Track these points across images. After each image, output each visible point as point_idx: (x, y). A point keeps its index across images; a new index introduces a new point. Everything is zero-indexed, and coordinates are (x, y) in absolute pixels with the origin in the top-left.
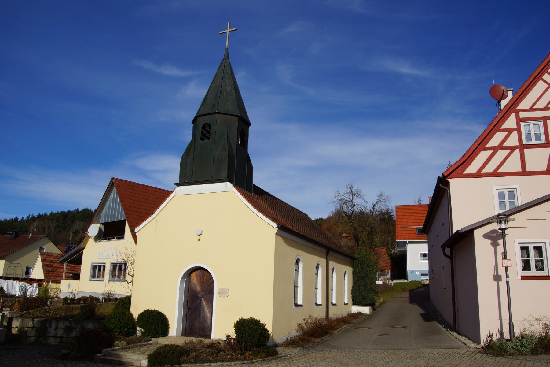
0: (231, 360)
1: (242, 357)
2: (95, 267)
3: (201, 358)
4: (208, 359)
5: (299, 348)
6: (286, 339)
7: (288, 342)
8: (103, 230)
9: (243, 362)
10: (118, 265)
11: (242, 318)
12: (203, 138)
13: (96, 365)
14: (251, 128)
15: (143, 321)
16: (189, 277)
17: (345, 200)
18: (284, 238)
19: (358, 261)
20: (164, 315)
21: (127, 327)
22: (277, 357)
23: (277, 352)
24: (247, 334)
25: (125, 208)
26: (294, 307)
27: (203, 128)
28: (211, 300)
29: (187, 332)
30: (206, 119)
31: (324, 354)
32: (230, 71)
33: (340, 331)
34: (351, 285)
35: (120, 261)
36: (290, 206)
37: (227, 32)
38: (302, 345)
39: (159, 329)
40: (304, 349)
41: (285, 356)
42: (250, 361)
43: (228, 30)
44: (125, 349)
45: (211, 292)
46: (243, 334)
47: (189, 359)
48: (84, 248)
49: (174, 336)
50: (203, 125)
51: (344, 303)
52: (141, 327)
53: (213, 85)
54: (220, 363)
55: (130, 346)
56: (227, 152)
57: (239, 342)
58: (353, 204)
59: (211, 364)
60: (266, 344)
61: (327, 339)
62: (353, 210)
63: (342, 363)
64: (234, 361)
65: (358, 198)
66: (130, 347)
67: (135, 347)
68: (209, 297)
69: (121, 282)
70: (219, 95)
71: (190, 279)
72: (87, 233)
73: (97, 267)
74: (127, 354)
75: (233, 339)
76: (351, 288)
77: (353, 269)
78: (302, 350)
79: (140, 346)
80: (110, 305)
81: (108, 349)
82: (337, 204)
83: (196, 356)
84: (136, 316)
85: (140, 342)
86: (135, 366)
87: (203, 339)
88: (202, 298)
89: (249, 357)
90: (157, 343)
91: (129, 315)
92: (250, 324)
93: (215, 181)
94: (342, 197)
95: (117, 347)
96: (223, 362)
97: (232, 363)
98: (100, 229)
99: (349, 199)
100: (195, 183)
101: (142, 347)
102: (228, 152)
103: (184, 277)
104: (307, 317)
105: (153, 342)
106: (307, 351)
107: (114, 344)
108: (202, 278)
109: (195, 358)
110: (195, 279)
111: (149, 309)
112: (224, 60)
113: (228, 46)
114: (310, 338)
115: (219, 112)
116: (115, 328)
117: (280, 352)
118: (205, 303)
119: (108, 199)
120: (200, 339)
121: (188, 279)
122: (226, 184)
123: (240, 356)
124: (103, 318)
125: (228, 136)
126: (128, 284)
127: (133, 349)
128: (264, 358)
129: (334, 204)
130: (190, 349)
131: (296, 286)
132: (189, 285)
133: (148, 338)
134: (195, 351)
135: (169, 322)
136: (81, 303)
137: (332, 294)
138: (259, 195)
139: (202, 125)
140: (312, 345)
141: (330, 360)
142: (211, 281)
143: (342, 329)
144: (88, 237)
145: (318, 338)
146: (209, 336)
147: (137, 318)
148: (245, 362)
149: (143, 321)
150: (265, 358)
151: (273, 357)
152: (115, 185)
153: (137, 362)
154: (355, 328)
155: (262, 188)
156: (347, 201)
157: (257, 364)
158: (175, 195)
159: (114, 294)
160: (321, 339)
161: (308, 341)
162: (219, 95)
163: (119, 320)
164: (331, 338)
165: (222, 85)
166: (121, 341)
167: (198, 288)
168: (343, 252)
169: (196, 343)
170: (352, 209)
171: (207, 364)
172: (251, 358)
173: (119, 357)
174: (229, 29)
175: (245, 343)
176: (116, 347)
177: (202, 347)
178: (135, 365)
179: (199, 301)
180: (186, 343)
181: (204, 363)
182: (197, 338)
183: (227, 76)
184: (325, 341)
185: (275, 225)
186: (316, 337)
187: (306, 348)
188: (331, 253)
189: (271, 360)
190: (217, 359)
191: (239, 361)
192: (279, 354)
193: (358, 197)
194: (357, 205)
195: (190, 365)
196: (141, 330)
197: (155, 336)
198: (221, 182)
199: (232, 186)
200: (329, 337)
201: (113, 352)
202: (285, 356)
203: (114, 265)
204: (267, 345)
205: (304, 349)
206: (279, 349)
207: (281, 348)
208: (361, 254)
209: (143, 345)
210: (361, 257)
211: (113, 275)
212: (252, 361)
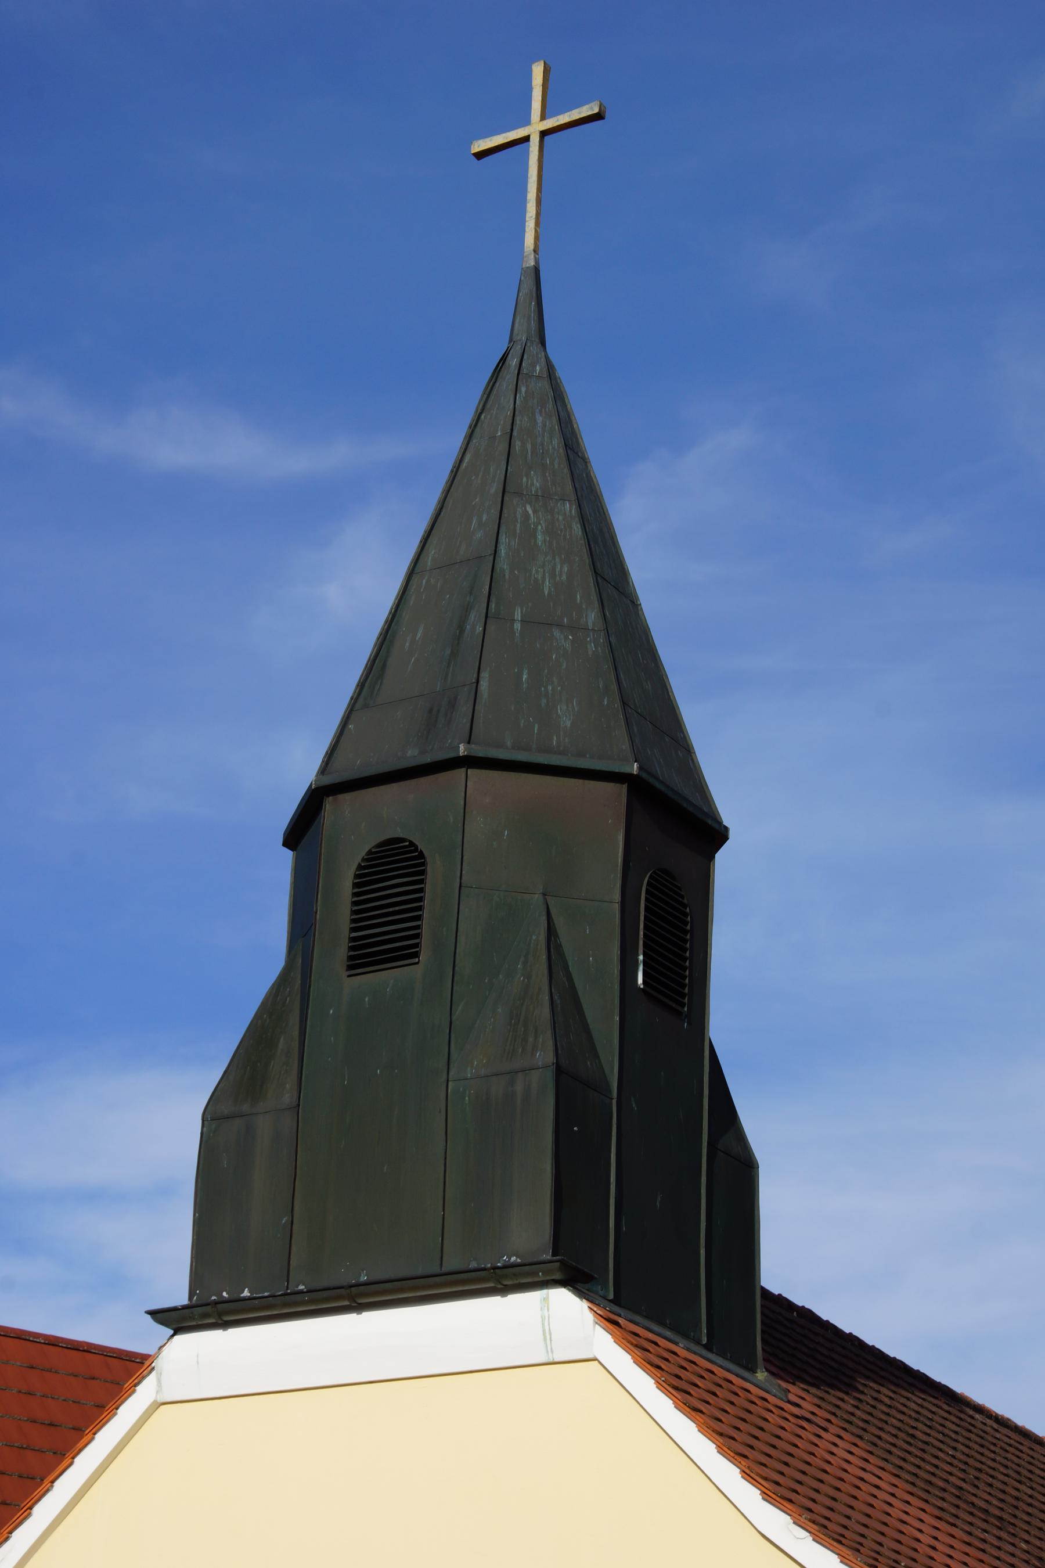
27: (364, 880)
32: (557, 442)
37: (526, 139)
43: (535, 127)
50: (363, 853)
53: (431, 552)
56: (544, 1056)
70: (475, 624)
100: (311, 1302)
102: (550, 1058)
112: (513, 362)
122: (546, 1299)
125: (551, 932)
138: (815, 1382)
139: (358, 860)
155: (846, 1324)
158: (157, 1405)
162: (475, 624)
165: (503, 550)
174: (543, 117)
183: (535, 482)
198: (504, 1290)
199: (590, 1317)
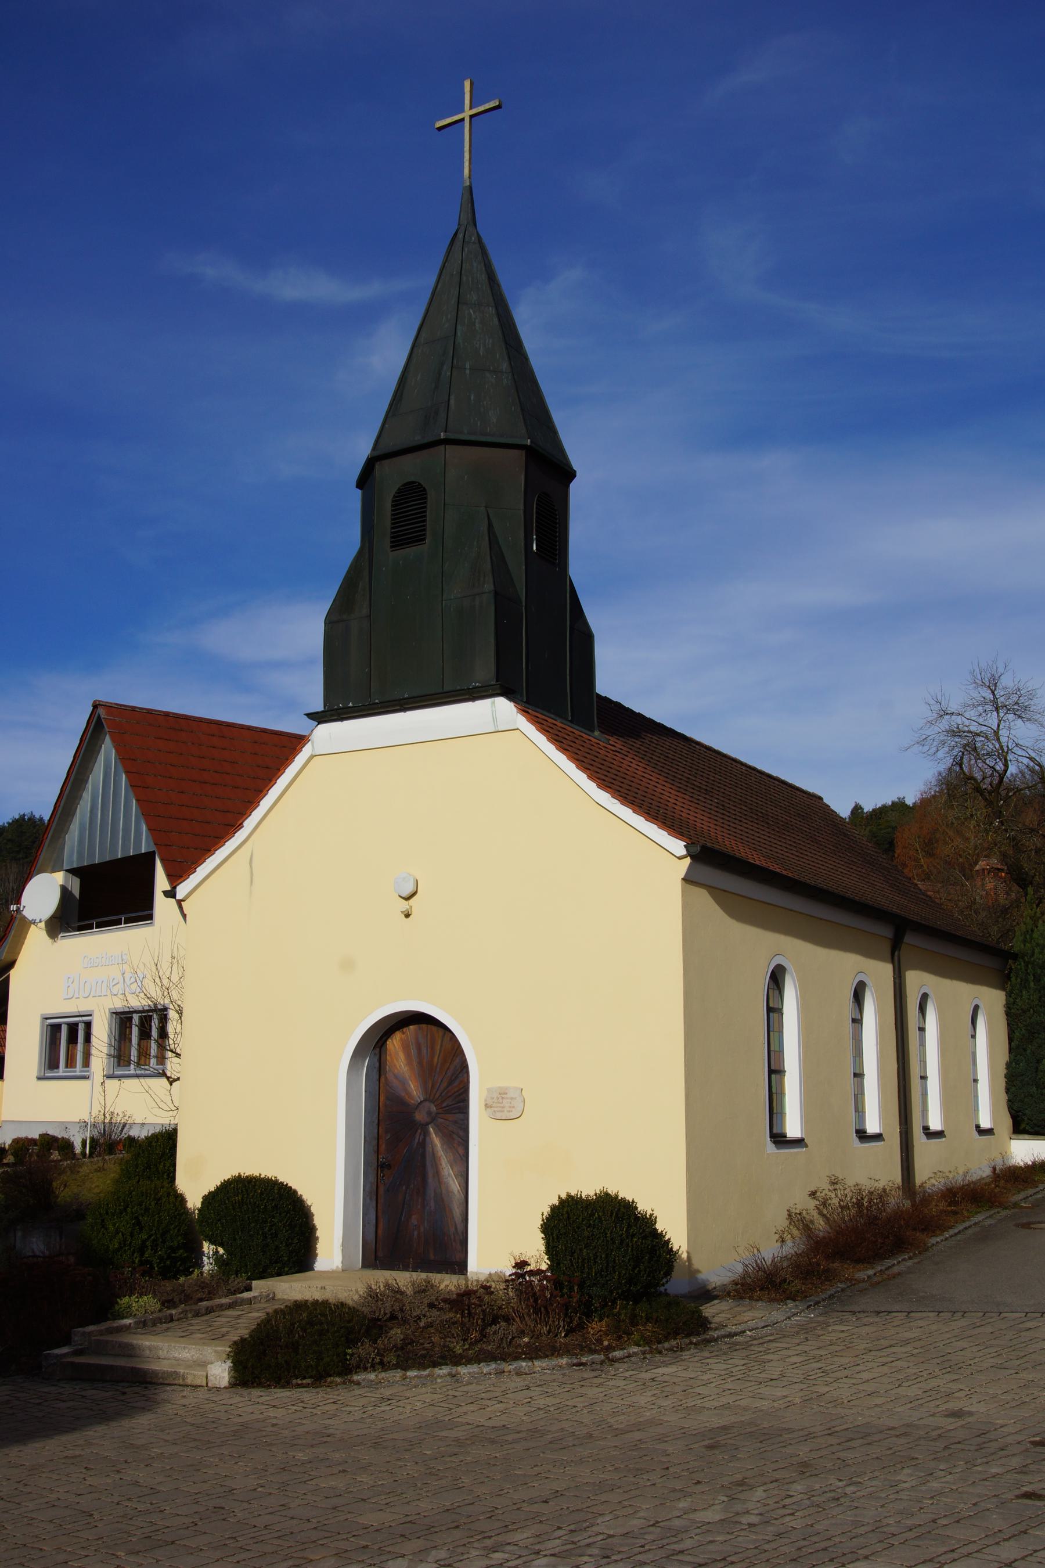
0: (533, 1353)
1: (576, 1338)
2: (55, 1029)
3: (424, 1349)
4: (450, 1350)
5: (791, 1304)
6: (740, 1269)
7: (749, 1280)
8: (76, 893)
9: (575, 1361)
10: (136, 1018)
11: (569, 1195)
12: (399, 541)
13: (46, 1390)
14: (576, 490)
15: (219, 1220)
16: (378, 1049)
17: (969, 732)
18: (718, 894)
19: (1027, 964)
20: (295, 1192)
21: (164, 1242)
22: (703, 1337)
23: (706, 1318)
24: (588, 1254)
25: (149, 810)
26: (771, 1148)
27: (397, 503)
28: (461, 1133)
29: (380, 1254)
30: (408, 468)
31: (883, 1327)
32: (483, 277)
33: (959, 1237)
34: (1004, 1057)
35: (137, 1002)
36: (750, 767)
37: (463, 120)
38: (803, 1292)
39: (277, 1248)
40: (808, 1307)
41: (736, 1334)
42: (602, 1357)
43: (467, 113)
44: (154, 1325)
45: (461, 1104)
46: (572, 1254)
47: (378, 1354)
48: (11, 964)
49: (334, 1268)
51: (978, 1127)
52: (212, 1242)
54: (493, 1366)
55: (173, 1312)
56: (489, 587)
57: (558, 1284)
58: (1001, 747)
59: (459, 1368)
60: (662, 1289)
61: (902, 1267)
62: (1003, 767)
63: (947, 1365)
64: (541, 1357)
65: (1020, 720)
66: (171, 1315)
67: (189, 1315)
68: (456, 1122)
69: (142, 1080)
71: (382, 1059)
72: (18, 910)
73: (64, 1030)
74: (160, 1344)
75: (539, 1272)
76: (1002, 1070)
77: (1009, 995)
78: (803, 1311)
79: (209, 1311)
80: (112, 1166)
81: (91, 1328)
82: (938, 750)
83: (407, 1342)
84: (194, 1201)
85: (211, 1295)
86: (187, 1386)
87: (436, 1278)
88: (427, 1124)
89: (600, 1341)
90: (271, 1298)
91: (172, 1199)
92: (599, 1218)
93: (453, 696)
94: (959, 720)
95: (126, 1317)
96: (504, 1360)
97: (537, 1363)
98: (65, 891)
99: (984, 728)
101: (217, 1314)
103: (359, 1053)
104: (824, 1185)
105: (256, 1294)
106: (820, 1315)
107: (117, 1307)
108: (424, 1050)
109: (402, 1348)
110: (402, 1056)
111: (240, 1175)
112: (461, 236)
113: (469, 177)
114: (836, 1265)
115: (451, 436)
116: (122, 1248)
117: (716, 1319)
118: (442, 1145)
119: (87, 781)
120: (424, 1275)
121: (377, 1057)
122: (494, 703)
123: (565, 1336)
124: (78, 1213)
125: (490, 525)
126: (171, 1085)
127: (184, 1325)
128: (653, 1344)
129: (926, 748)
130: (385, 1314)
131: (777, 1068)
132: (383, 1079)
133: (240, 1281)
134: (405, 1321)
135: (315, 1218)
136: (7, 1165)
137: (924, 1094)
140: (843, 1290)
141: (904, 1349)
142: (457, 1061)
143: (966, 1228)
144: (26, 924)
145: (868, 1263)
146: (460, 1266)
147: (199, 1210)
148: (584, 1360)
149: (219, 1220)
150: (659, 1342)
151: (687, 1341)
152: (107, 730)
153: (195, 1372)
154: (1017, 1225)
156: (978, 735)
157: (626, 1366)
158: (312, 757)
159: (124, 1125)
160: (879, 1268)
161: (828, 1276)
163: (137, 1218)
164: (919, 1262)
165: (459, 334)
166: (141, 1295)
167: (414, 1091)
168: (959, 933)
169: (409, 1291)
170: (1000, 767)
171: (444, 1370)
172: (606, 1343)
173: (130, 1356)
174: (471, 108)
175: (581, 1286)
176: (123, 1318)
177: (431, 1306)
178: (189, 1381)
179: (418, 1138)
180: (372, 1295)
181: (434, 1367)
182: (414, 1274)
184: (894, 1276)
185: (678, 846)
186: (859, 1261)
187: (817, 1303)
188: (909, 939)
189: (682, 1350)
190: (481, 1350)
191: (561, 1356)
192: (711, 1329)
193: (1020, 717)
194: (1016, 750)
195: (383, 1374)
196: (216, 1252)
197: (264, 1271)
199: (515, 710)
200: (910, 1258)
201: (109, 1338)
202: (736, 1334)
203: (123, 1019)
204: (667, 1294)
205: (808, 1307)
206: (709, 1310)
207: (724, 1303)
208: (1035, 935)
209: (222, 1307)
210: (1037, 950)
211: (120, 1057)
212: (610, 1355)
